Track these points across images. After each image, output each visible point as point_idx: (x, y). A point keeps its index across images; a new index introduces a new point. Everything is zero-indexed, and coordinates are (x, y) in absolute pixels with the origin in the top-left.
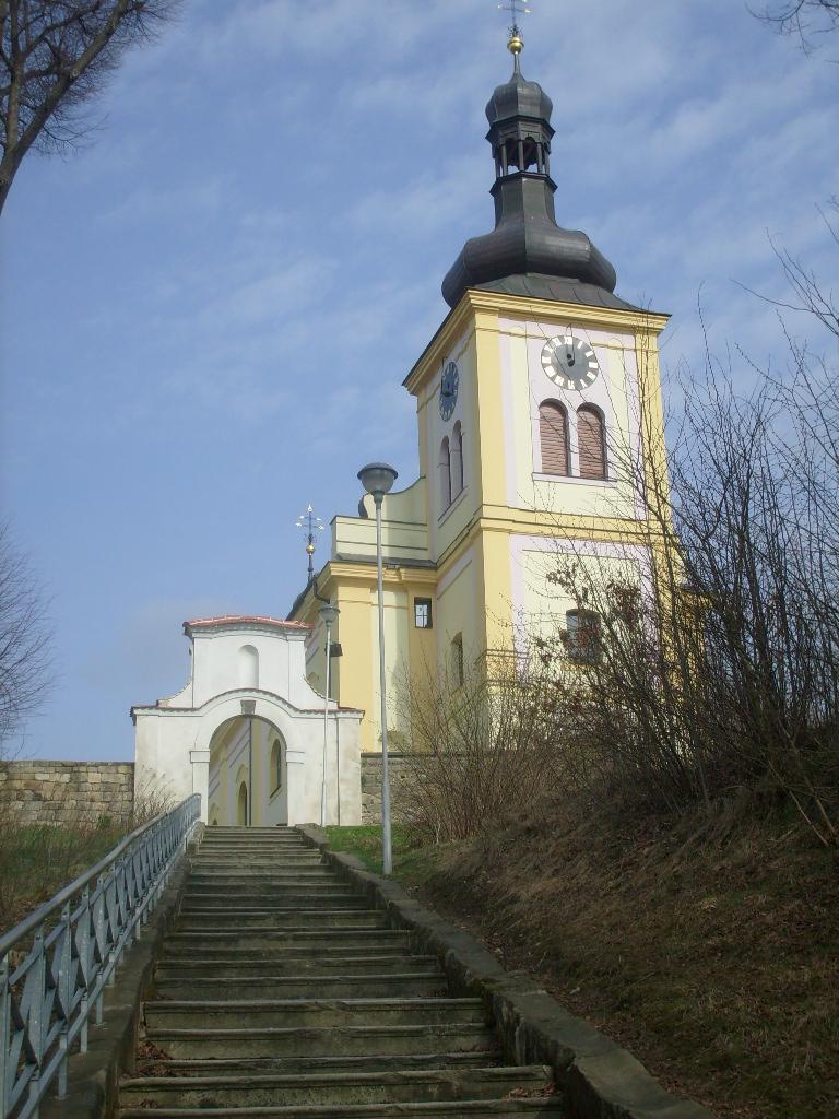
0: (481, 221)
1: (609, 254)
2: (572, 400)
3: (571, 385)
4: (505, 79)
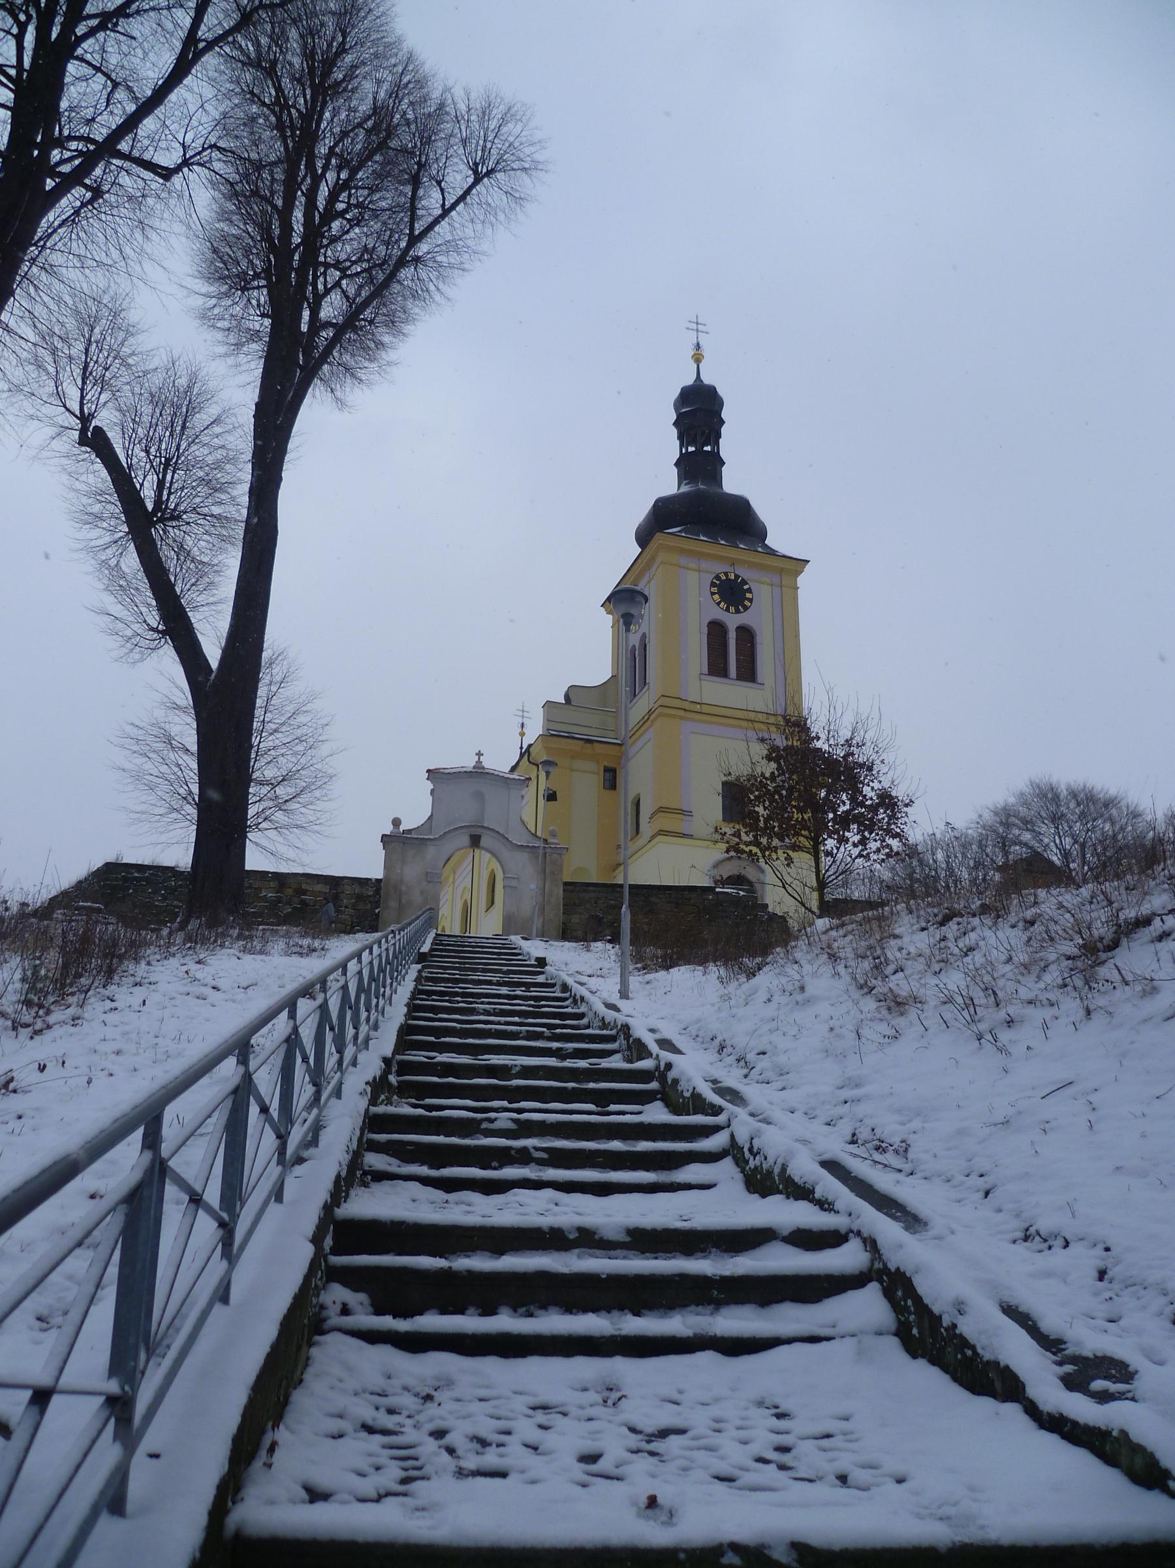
0: (668, 484)
1: (763, 510)
2: (733, 621)
3: (732, 609)
4: (690, 380)
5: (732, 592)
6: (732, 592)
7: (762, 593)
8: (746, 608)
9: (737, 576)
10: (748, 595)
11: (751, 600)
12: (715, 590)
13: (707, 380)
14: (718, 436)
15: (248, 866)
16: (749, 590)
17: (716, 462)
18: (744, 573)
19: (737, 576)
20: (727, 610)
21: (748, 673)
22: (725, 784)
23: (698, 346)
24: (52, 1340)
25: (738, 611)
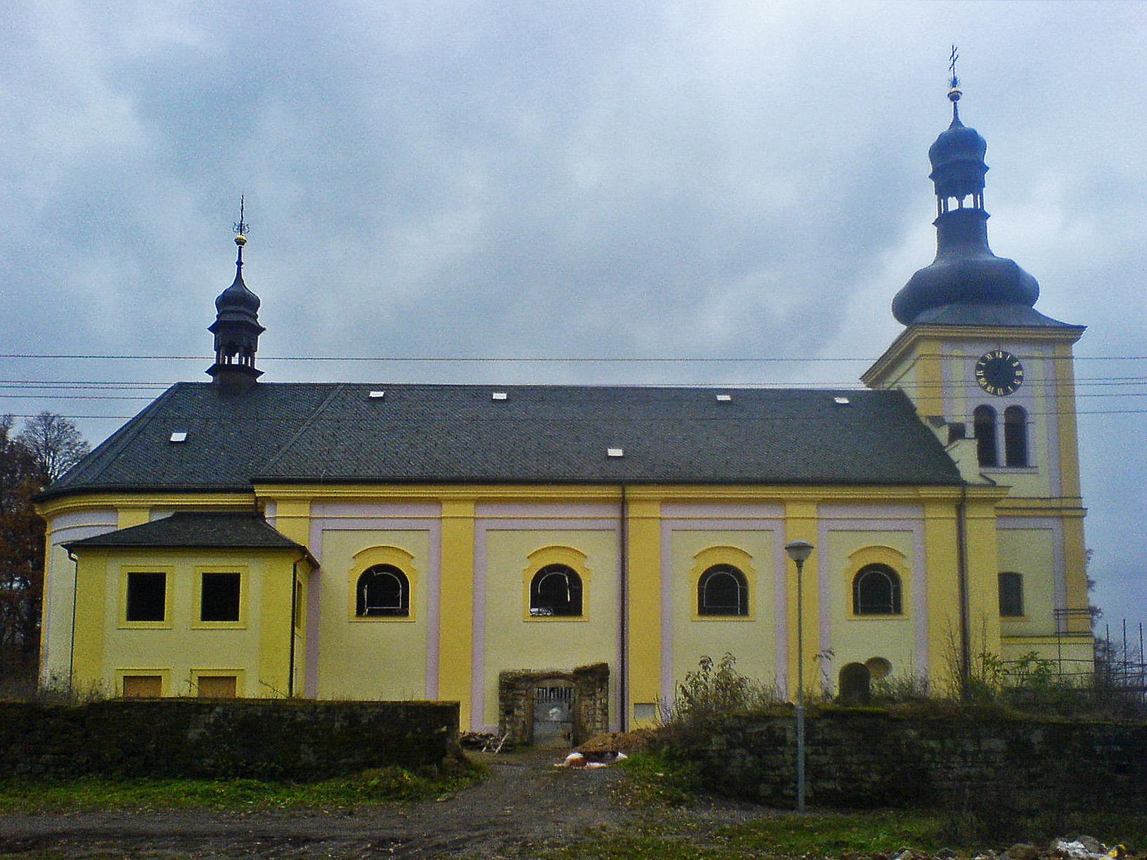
2: (1000, 404)
3: (1000, 391)
4: (944, 126)
5: (1000, 374)
6: (1000, 374)
7: (1034, 368)
8: (1015, 387)
9: (1005, 354)
10: (1018, 373)
11: (1020, 378)
12: (980, 373)
13: (967, 122)
14: (982, 185)
15: (55, 661)
16: (1019, 368)
17: (978, 217)
18: (1014, 351)
19: (1005, 354)
20: (995, 393)
21: (1018, 457)
22: (1000, 575)
23: (954, 83)
24: (980, 480)
25: (1007, 392)
